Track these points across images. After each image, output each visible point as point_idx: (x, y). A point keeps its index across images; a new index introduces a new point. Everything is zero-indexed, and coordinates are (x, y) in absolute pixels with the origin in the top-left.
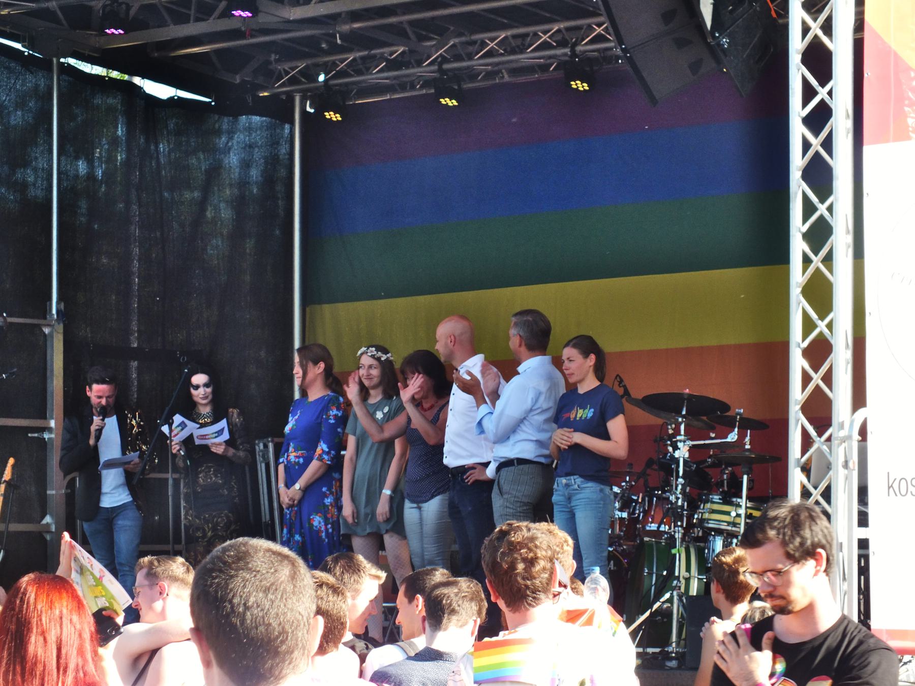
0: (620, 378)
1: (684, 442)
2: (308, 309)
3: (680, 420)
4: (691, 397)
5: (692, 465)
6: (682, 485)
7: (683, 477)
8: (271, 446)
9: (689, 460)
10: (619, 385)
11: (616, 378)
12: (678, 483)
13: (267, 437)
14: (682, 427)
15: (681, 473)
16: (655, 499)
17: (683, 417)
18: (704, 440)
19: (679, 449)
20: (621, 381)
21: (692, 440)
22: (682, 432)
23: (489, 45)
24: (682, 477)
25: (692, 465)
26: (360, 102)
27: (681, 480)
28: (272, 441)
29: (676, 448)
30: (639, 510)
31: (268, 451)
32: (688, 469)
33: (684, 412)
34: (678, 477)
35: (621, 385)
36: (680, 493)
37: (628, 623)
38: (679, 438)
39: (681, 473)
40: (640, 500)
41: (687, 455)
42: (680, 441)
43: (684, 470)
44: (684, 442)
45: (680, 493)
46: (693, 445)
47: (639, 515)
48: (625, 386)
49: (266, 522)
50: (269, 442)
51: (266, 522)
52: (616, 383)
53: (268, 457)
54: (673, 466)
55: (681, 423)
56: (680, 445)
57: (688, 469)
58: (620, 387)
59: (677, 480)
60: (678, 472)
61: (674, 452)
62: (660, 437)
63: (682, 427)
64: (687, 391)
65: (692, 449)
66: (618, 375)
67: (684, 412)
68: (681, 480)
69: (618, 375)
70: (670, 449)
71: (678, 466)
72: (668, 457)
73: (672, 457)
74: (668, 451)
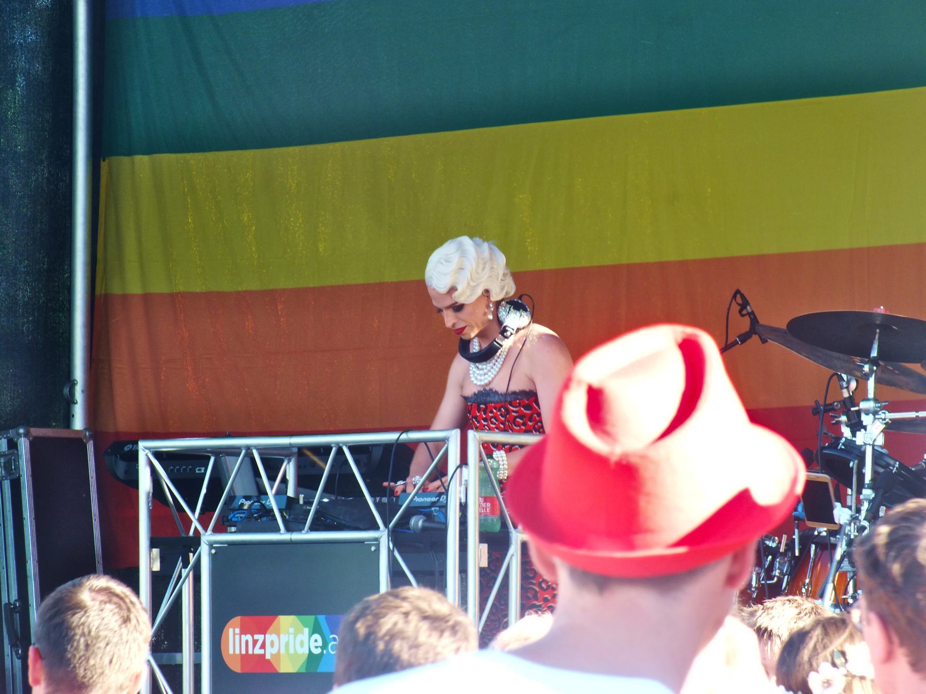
0: (743, 296)
1: (875, 413)
2: (104, 165)
3: (866, 368)
4: (888, 322)
5: (892, 462)
6: (870, 501)
7: (873, 487)
8: (24, 445)
9: (884, 451)
10: (740, 312)
11: (734, 297)
12: (862, 497)
13: (15, 426)
14: (871, 383)
15: (868, 478)
16: (813, 547)
17: (874, 362)
18: (917, 411)
19: (865, 428)
20: (745, 304)
21: (891, 410)
22: (871, 395)
23: (277, 530)
24: (870, 487)
25: (892, 462)
26: (3, 613)
27: (868, 493)
28: (26, 435)
29: (857, 425)
30: (781, 570)
31: (18, 457)
32: (881, 470)
33: (874, 354)
34: (861, 486)
35: (744, 312)
36: (864, 519)
37: (797, 595)
38: (863, 405)
39: (868, 478)
40: (782, 550)
41: (880, 441)
42: (867, 412)
43: (875, 473)
44: (875, 413)
45: (864, 519)
46: (894, 421)
47: (780, 581)
48: (752, 314)
49: (9, 603)
50: (19, 435)
51: (9, 603)
52: (735, 308)
53: (17, 468)
54: (851, 464)
55: (866, 377)
56: (866, 419)
57: (881, 470)
58: (743, 316)
59: (859, 492)
60: (861, 476)
61: (854, 435)
62: (826, 405)
63: (871, 383)
64: (881, 310)
65: (891, 429)
66: (738, 292)
67: (874, 354)
68: (868, 493)
69: (738, 292)
70: (846, 432)
71: (862, 464)
72: (841, 446)
73: (850, 444)
74: (841, 435)
